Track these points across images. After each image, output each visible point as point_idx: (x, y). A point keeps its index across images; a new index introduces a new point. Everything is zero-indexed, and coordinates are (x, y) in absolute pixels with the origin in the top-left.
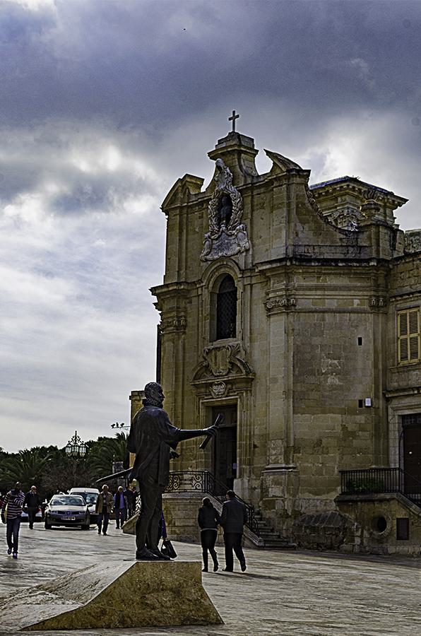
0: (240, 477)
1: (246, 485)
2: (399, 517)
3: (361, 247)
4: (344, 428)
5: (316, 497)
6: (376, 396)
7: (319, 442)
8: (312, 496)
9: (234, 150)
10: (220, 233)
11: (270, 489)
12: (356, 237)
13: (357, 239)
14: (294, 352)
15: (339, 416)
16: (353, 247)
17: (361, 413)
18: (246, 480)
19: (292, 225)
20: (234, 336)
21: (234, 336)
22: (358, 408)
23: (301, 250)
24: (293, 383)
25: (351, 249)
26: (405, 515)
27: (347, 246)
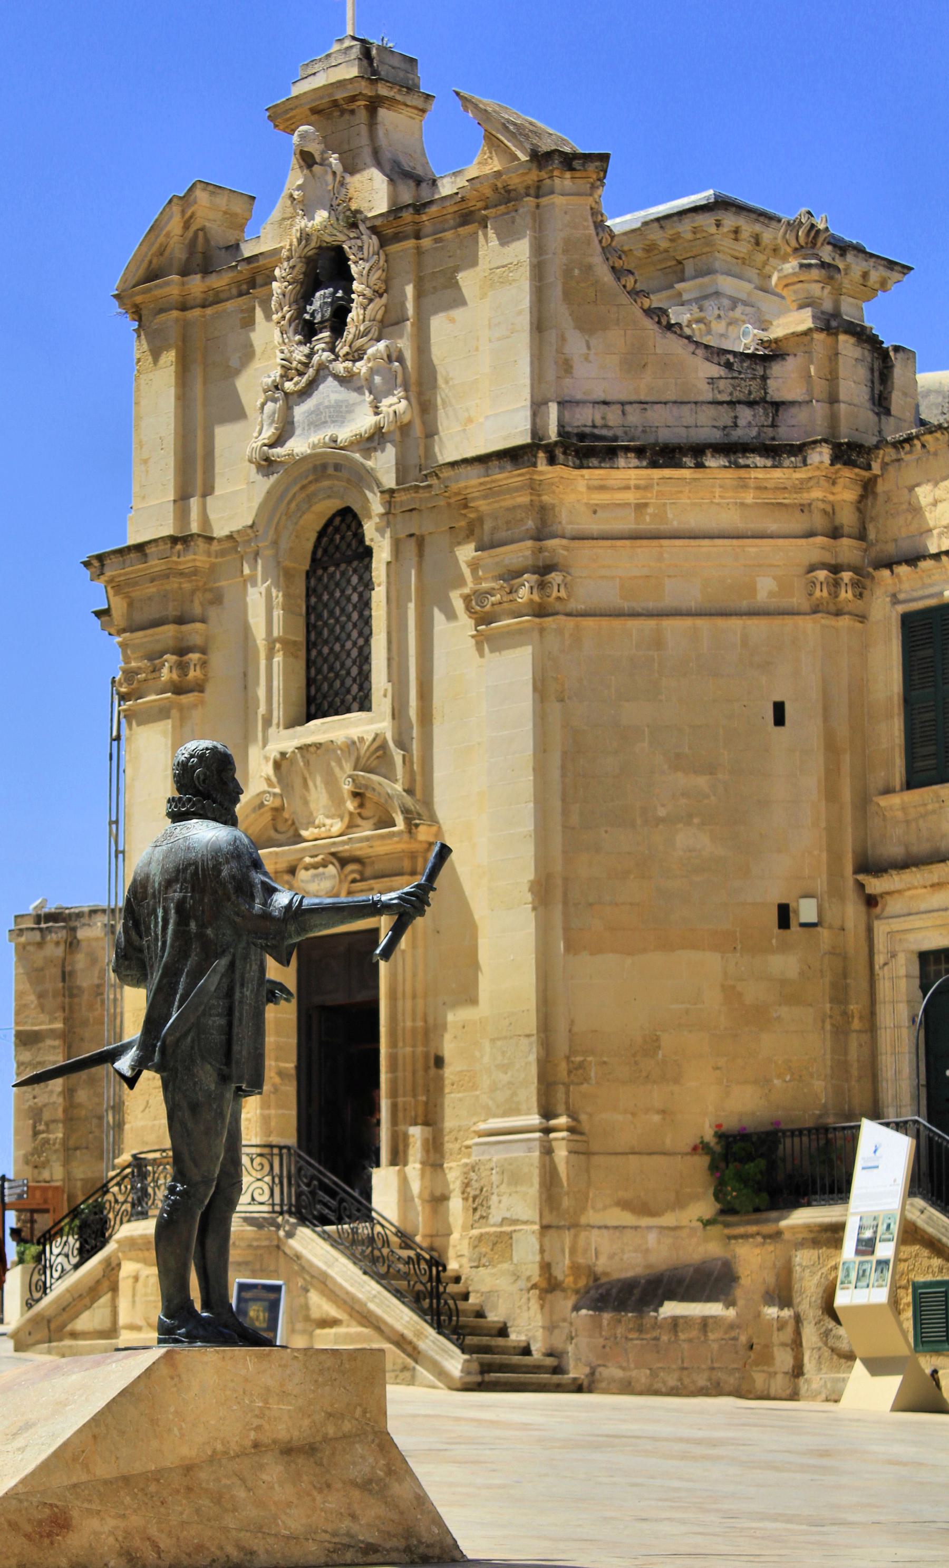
0: (394, 1162)
1: (416, 1186)
2: (921, 1279)
3: (777, 406)
4: (731, 994)
5: (645, 1221)
6: (835, 892)
7: (651, 1045)
8: (627, 1218)
9: (353, 99)
10: (311, 372)
11: (494, 1198)
12: (760, 371)
13: (764, 378)
14: (564, 753)
15: (712, 961)
16: (751, 404)
17: (784, 948)
18: (413, 1168)
19: (552, 335)
20: (364, 704)
21: (364, 704)
22: (776, 930)
23: (584, 418)
24: (565, 852)
25: (745, 415)
26: (406, 1327)
27: (731, 403)
